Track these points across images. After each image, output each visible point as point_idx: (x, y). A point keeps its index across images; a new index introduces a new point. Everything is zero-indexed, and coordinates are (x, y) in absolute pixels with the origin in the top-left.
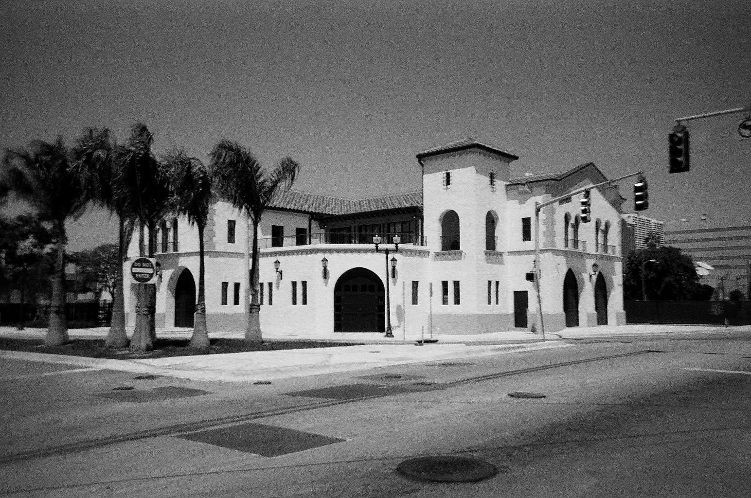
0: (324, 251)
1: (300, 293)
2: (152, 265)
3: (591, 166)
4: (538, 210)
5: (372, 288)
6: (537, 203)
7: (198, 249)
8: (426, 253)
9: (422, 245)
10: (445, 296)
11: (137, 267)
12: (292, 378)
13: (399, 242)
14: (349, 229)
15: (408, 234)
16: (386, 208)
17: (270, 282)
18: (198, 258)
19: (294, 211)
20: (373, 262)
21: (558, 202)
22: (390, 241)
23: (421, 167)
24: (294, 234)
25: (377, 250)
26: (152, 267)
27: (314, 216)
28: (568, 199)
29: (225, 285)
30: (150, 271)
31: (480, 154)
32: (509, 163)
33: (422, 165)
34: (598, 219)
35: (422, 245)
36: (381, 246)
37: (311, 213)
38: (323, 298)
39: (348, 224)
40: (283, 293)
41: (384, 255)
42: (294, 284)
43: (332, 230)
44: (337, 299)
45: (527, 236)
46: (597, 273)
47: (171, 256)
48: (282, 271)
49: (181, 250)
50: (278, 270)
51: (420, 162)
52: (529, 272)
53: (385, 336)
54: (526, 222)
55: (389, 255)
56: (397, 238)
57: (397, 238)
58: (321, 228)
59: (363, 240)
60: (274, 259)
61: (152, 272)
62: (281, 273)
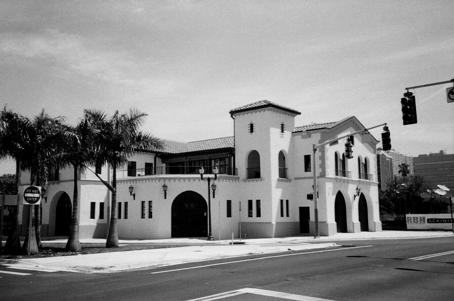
0: (165, 179)
2: (39, 191)
3: (354, 118)
4: (315, 150)
7: (73, 178)
10: (250, 211)
11: (28, 193)
13: (203, 172)
14: (183, 164)
15: (224, 167)
16: (211, 148)
17: (258, 199)
18: (73, 183)
21: (329, 144)
22: (211, 172)
23: (233, 120)
24: (144, 167)
25: (202, 178)
26: (39, 193)
28: (335, 142)
30: (37, 195)
31: (274, 111)
32: (294, 117)
33: (234, 119)
34: (360, 155)
35: (234, 174)
39: (183, 159)
42: (143, 203)
43: (171, 164)
45: (307, 168)
46: (360, 194)
48: (135, 194)
50: (132, 193)
51: (232, 116)
52: (309, 194)
54: (307, 159)
55: (210, 182)
56: (216, 171)
58: (163, 163)
61: (39, 196)
62: (134, 195)
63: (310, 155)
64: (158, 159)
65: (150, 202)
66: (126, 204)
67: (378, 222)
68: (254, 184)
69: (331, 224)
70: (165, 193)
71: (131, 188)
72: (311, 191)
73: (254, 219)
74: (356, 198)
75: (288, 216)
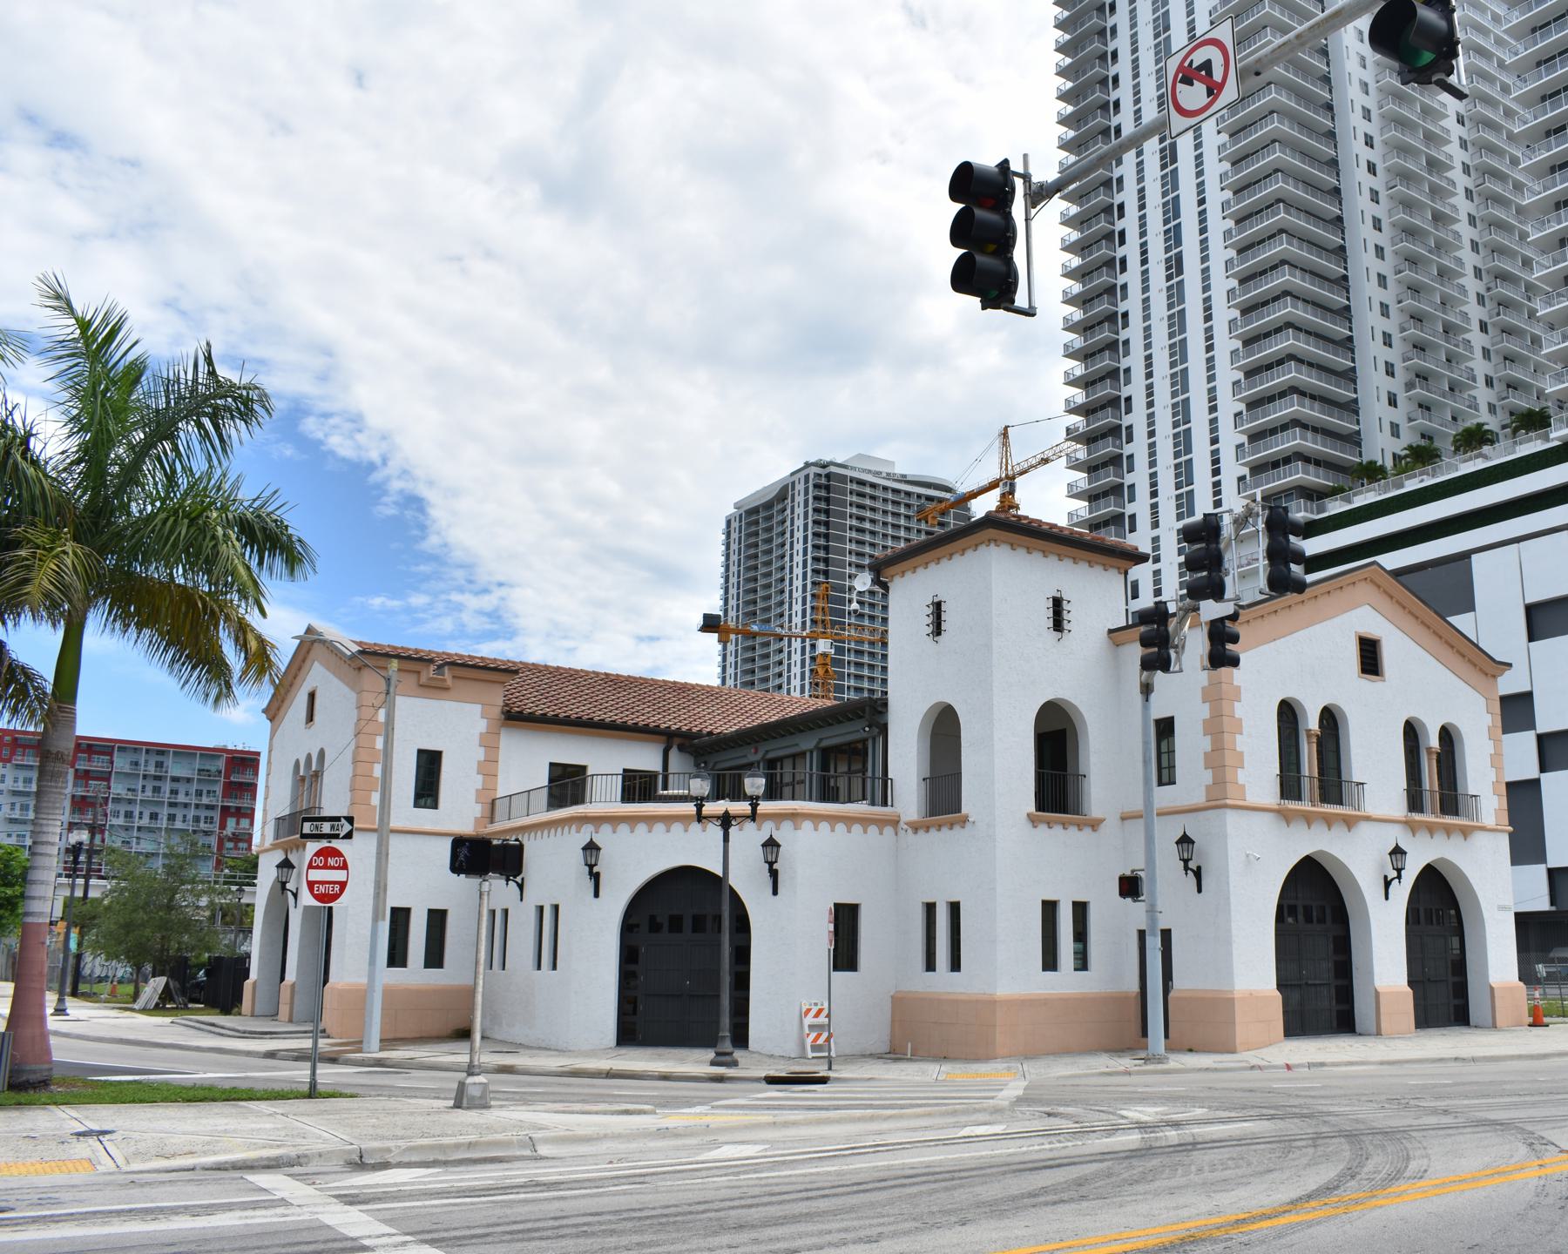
8: (895, 823)
9: (885, 804)
11: (318, 867)
12: (1225, 1185)
18: (395, 842)
22: (737, 794)
25: (700, 817)
27: (671, 739)
29: (930, 908)
30: (316, 875)
35: (885, 804)
36: (710, 808)
41: (715, 831)
42: (541, 909)
44: (629, 955)
48: (1199, 868)
52: (1128, 873)
53: (713, 1063)
56: (755, 784)
57: (755, 784)
62: (1198, 874)
63: (258, 754)
65: (556, 908)
67: (1511, 989)
68: (941, 841)
69: (1252, 997)
70: (774, 874)
71: (591, 848)
73: (943, 981)
74: (1391, 889)
75: (1082, 963)
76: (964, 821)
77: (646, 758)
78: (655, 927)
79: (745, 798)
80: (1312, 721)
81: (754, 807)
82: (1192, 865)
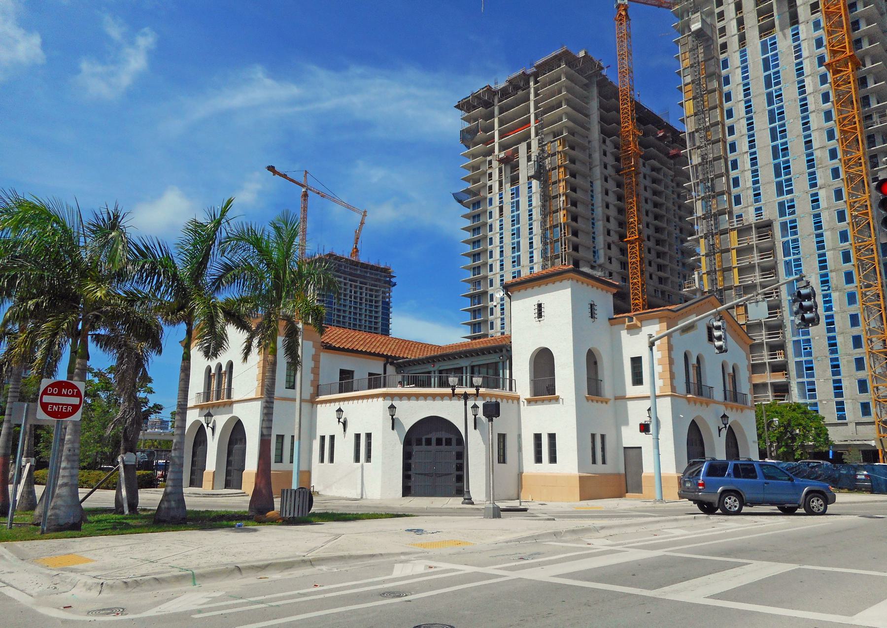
0: (392, 396)
1: (363, 448)
4: (652, 345)
5: (449, 442)
6: (650, 336)
11: (52, 394)
19: (366, 353)
20: (452, 411)
26: (78, 395)
27: (389, 360)
29: (593, 436)
33: (510, 297)
37: (387, 357)
38: (389, 452)
40: (344, 448)
42: (358, 436)
47: (225, 404)
49: (235, 396)
53: (463, 503)
59: (443, 384)
60: (337, 406)
64: (389, 367)
66: (332, 438)
71: (392, 407)
72: (644, 419)
75: (604, 462)
76: (557, 399)
77: (377, 367)
78: (419, 442)
79: (448, 386)
80: (693, 361)
81: (478, 390)
82: (342, 420)
